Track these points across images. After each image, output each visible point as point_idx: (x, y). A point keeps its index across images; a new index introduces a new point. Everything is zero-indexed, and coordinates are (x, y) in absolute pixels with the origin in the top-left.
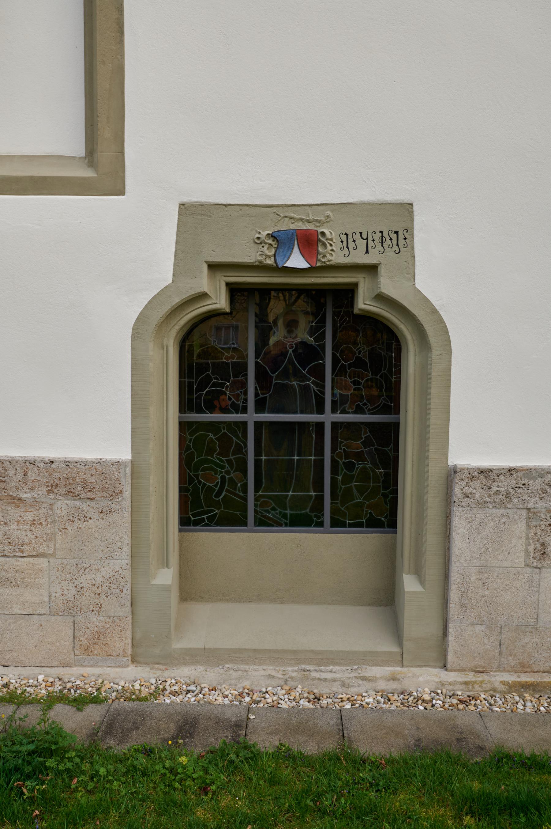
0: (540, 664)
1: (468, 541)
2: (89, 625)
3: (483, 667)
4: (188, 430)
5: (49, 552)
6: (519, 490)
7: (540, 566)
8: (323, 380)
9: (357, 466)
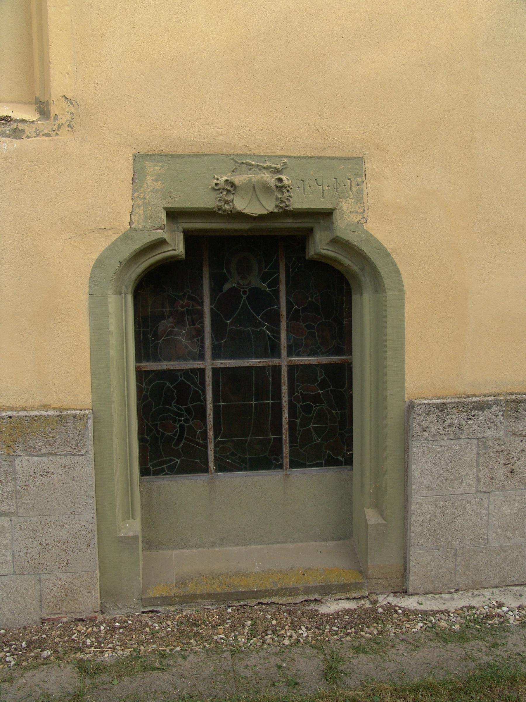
0: (490, 580)
1: (425, 472)
2: (55, 582)
3: (441, 589)
4: (145, 380)
5: (10, 511)
6: (470, 422)
7: (489, 490)
8: (278, 326)
9: (314, 408)
